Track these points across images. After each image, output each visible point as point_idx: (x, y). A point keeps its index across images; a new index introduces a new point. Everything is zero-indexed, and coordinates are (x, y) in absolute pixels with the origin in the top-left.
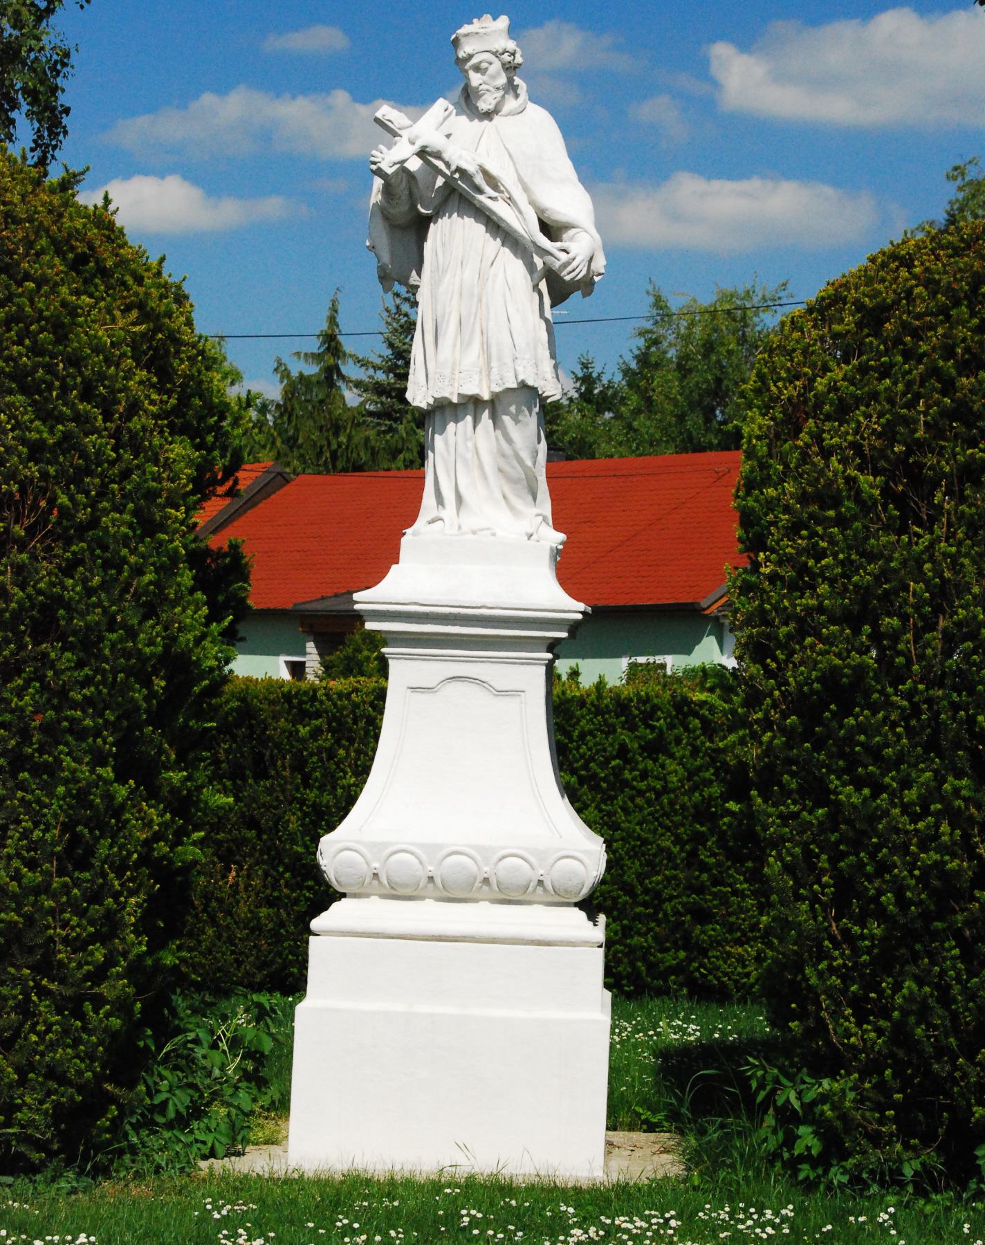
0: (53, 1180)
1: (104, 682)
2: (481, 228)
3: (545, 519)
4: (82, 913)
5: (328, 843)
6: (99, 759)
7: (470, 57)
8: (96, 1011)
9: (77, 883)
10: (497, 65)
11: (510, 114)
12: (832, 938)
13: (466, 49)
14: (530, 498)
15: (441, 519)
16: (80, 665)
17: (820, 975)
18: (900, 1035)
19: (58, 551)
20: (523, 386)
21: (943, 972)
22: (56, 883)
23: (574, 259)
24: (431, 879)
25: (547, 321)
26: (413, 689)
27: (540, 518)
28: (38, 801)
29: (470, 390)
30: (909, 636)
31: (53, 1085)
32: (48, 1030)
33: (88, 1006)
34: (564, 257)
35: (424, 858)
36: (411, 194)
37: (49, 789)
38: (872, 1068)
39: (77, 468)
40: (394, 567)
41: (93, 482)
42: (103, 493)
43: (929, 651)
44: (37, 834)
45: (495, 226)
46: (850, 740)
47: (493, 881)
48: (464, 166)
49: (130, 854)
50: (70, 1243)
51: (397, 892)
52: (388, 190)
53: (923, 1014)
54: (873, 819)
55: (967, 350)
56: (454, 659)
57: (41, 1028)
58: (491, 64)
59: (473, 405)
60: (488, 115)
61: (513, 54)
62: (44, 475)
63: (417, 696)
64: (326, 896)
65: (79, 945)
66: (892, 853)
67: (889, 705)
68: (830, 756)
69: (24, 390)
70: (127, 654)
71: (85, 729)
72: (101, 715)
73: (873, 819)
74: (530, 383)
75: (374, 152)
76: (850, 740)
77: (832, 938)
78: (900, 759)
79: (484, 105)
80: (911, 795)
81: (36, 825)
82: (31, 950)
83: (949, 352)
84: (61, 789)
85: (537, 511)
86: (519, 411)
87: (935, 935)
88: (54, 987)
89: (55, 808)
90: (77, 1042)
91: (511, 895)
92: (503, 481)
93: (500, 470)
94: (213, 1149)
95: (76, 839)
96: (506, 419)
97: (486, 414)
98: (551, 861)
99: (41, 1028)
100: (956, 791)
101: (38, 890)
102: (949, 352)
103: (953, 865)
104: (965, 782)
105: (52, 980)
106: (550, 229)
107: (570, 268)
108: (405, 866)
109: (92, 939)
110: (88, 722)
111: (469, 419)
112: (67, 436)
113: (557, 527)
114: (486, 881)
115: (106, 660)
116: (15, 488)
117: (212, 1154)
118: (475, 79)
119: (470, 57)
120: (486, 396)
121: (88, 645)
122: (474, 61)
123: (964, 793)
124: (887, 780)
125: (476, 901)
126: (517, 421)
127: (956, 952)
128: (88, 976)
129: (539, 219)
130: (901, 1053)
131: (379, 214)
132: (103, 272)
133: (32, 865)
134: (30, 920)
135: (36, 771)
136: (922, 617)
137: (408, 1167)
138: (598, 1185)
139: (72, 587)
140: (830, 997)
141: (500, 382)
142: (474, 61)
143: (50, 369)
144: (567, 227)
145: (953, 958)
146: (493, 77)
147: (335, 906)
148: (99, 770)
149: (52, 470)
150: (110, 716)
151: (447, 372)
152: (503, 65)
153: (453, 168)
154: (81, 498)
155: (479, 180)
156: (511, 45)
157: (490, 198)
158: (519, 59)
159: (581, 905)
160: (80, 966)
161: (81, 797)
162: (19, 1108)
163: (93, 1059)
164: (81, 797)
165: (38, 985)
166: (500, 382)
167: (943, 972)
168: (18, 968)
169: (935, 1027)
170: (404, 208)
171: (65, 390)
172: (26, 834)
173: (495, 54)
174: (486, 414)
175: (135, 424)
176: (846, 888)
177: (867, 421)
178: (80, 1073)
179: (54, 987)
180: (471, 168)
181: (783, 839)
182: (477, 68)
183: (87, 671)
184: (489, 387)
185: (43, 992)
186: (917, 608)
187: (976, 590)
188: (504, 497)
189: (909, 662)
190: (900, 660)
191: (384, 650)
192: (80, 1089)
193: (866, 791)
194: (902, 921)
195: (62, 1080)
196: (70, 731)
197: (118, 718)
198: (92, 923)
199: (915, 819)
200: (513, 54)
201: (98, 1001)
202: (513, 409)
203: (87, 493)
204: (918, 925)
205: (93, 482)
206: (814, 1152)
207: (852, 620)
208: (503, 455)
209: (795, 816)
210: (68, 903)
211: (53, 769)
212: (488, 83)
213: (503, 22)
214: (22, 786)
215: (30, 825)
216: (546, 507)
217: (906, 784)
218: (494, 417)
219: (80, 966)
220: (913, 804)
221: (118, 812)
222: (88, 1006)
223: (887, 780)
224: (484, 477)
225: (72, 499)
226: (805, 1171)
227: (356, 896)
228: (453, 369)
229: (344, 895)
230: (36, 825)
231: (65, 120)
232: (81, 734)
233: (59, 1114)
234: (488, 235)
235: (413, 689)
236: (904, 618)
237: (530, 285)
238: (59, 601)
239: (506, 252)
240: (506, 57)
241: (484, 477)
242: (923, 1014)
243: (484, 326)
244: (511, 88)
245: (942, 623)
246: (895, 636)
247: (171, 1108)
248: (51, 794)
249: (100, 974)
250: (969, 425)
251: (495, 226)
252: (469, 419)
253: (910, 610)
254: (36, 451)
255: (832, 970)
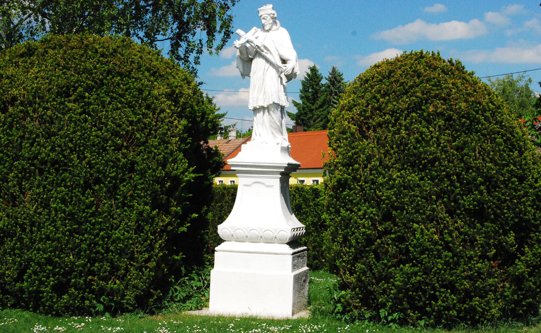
0: (137, 314)
1: (147, 184)
2: (264, 61)
4: (142, 245)
5: (220, 227)
6: (146, 204)
7: (262, 16)
8: (146, 270)
9: (140, 236)
10: (269, 18)
11: (275, 30)
12: (344, 253)
13: (261, 14)
14: (280, 134)
16: (140, 179)
17: (340, 262)
18: (359, 280)
19: (136, 149)
20: (274, 103)
21: (370, 262)
22: (134, 236)
24: (247, 236)
25: (284, 86)
26: (245, 185)
28: (129, 215)
29: (261, 104)
30: (361, 170)
31: (135, 289)
32: (133, 275)
33: (144, 269)
34: (285, 68)
35: (245, 231)
36: (247, 53)
37: (132, 211)
38: (354, 289)
39: (142, 127)
40: (240, 153)
41: (147, 131)
42: (150, 134)
43: (366, 174)
44: (129, 223)
45: (267, 60)
46: (345, 198)
47: (263, 237)
48: (258, 45)
49: (157, 229)
51: (239, 240)
52: (240, 52)
53: (364, 273)
54: (351, 219)
55: (384, 91)
56: (255, 177)
57: (132, 274)
59: (263, 108)
60: (268, 31)
61: (274, 14)
62: (133, 129)
63: (246, 187)
64: (219, 241)
65: (141, 253)
66: (355, 229)
67: (356, 189)
68: (341, 202)
69: (130, 107)
70: (153, 176)
71: (142, 196)
72: (147, 192)
73: (351, 219)
76: (345, 198)
77: (344, 253)
78: (358, 203)
79: (267, 28)
80: (360, 213)
81: (129, 221)
82: (127, 254)
83: (379, 92)
84: (135, 212)
86: (274, 110)
87: (367, 252)
88: (135, 264)
89: (134, 216)
90: (141, 278)
91: (269, 241)
92: (272, 129)
93: (271, 126)
94: (191, 308)
95: (139, 225)
96: (271, 112)
97: (266, 111)
98: (249, 230)
99: (132, 274)
100: (372, 212)
101: (128, 239)
102: (379, 92)
103: (369, 232)
104: (374, 210)
105: (134, 262)
106: (284, 61)
108: (240, 233)
109: (145, 251)
110: (142, 194)
111: (262, 112)
112: (139, 119)
114: (261, 237)
115: (147, 178)
116: (124, 133)
117: (191, 309)
118: (263, 21)
119: (262, 16)
120: (266, 106)
121: (143, 174)
122: (263, 17)
123: (374, 212)
124: (354, 209)
125: (260, 242)
126: (274, 113)
127: (373, 256)
128: (143, 261)
129: (280, 57)
130: (360, 284)
131: (239, 58)
132: (161, 76)
133: (128, 232)
134: (126, 246)
135: (129, 207)
136: (364, 164)
137: (234, 313)
139: (138, 159)
140: (343, 268)
142: (263, 17)
143: (137, 101)
144: (288, 60)
145: (372, 258)
146: (268, 21)
147: (223, 244)
148: (146, 207)
149: (135, 128)
150: (149, 192)
151: (255, 100)
154: (143, 135)
155: (262, 48)
156: (273, 12)
158: (276, 16)
159: (288, 244)
160: (141, 259)
161: (140, 214)
162: (126, 295)
163: (146, 283)
164: (140, 214)
165: (130, 263)
167: (370, 262)
168: (124, 259)
169: (368, 277)
170: (246, 56)
171: (140, 106)
172: (126, 223)
173: (269, 15)
174: (266, 111)
175: (162, 115)
176: (345, 239)
177: (356, 111)
178: (142, 286)
179: (135, 264)
180: (260, 45)
181: (330, 225)
182: (264, 19)
183: (142, 181)
185: (131, 265)
186: (363, 162)
187: (377, 157)
189: (361, 176)
190: (358, 176)
192: (142, 291)
193: (349, 212)
194: (358, 248)
195: (137, 288)
196: (138, 196)
197: (151, 193)
198: (145, 247)
199: (361, 220)
200: (274, 14)
201: (146, 268)
202: (272, 109)
203: (144, 134)
204: (362, 249)
205: (147, 131)
206: (340, 311)
207: (346, 165)
208: (272, 122)
209: (333, 219)
210: (138, 241)
211: (133, 206)
212: (267, 22)
213: (271, 6)
214: (125, 211)
215: (127, 221)
217: (359, 210)
218: (268, 112)
219: (141, 259)
220: (361, 216)
221: (153, 218)
222: (144, 269)
223: (354, 209)
224: (266, 128)
225: (140, 135)
226: (339, 316)
227: (228, 241)
229: (224, 241)
230: (129, 221)
231: (231, 35)
232: (141, 197)
233: (137, 298)
235: (245, 185)
236: (360, 165)
237: (277, 76)
238: (136, 162)
239: (271, 67)
240: (272, 15)
241: (266, 128)
242: (364, 273)
244: (275, 22)
245: (369, 166)
246: (357, 170)
247: (178, 297)
248: (133, 213)
249: (148, 260)
250: (381, 112)
251: (267, 60)
252: (262, 112)
253: (361, 163)
254: (131, 123)
255: (344, 261)
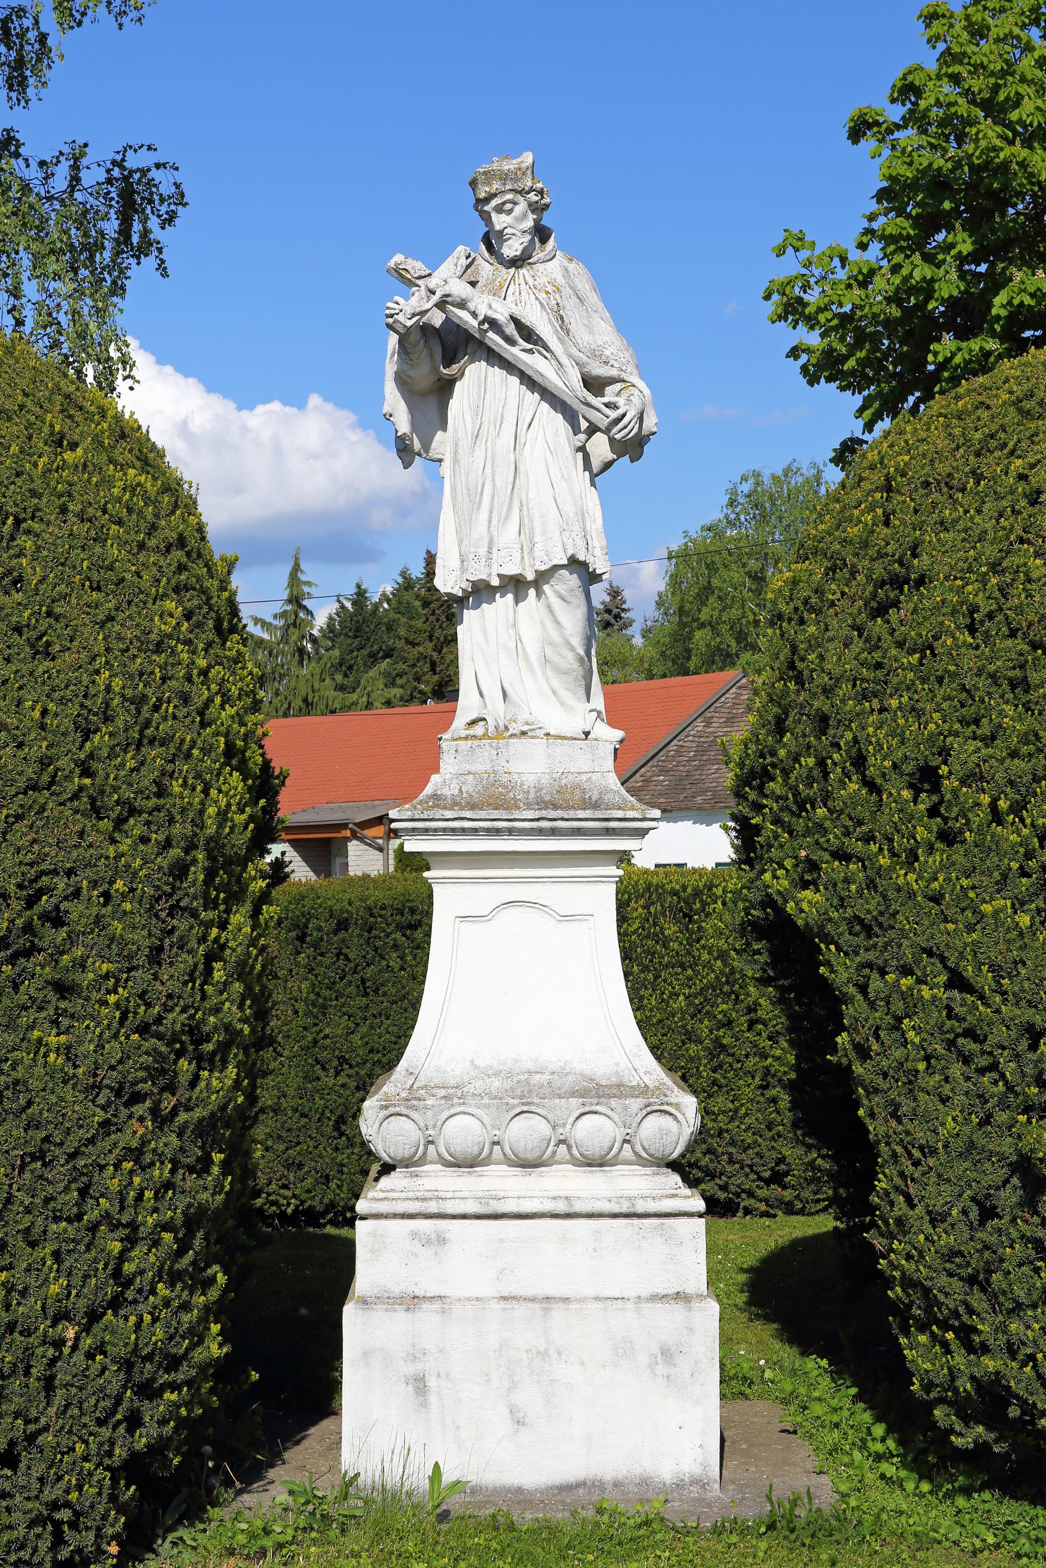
3: (599, 713)
14: (582, 692)
15: (484, 719)
23: (624, 415)
27: (595, 714)
50: (590, 1563)
58: (515, 203)
74: (582, 558)
75: (390, 304)
79: (512, 248)
85: (590, 706)
106: (594, 384)
107: (621, 425)
113: (613, 723)
138: (590, 1513)
141: (546, 558)
151: (483, 551)
152: (530, 205)
153: (481, 318)
157: (523, 350)
166: (546, 558)
173: (521, 192)
184: (533, 566)
188: (554, 692)
191: (426, 874)
216: (598, 701)
218: (539, 594)
228: (490, 548)
234: (524, 387)
239: (545, 406)
240: (533, 197)
241: (531, 669)
243: (524, 497)
